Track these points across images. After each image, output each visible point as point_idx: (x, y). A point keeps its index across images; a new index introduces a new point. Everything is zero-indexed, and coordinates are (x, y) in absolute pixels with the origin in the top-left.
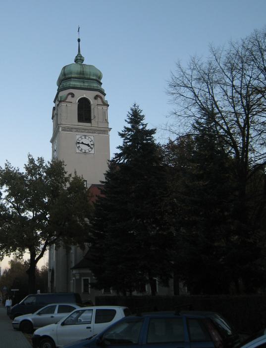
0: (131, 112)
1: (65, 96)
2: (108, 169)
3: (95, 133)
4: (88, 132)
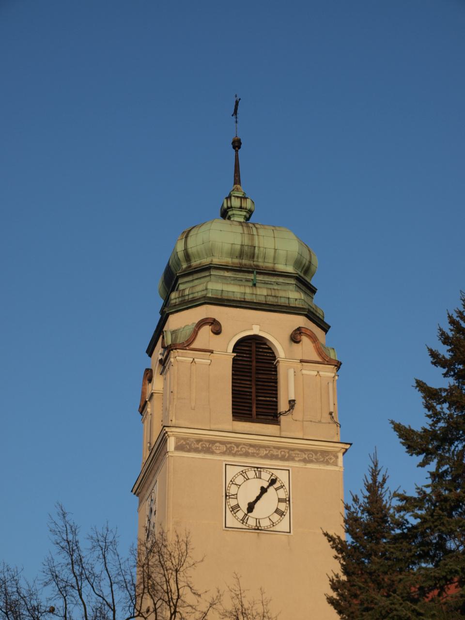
0: (430, 356)
1: (189, 332)
2: (336, 611)
3: (290, 459)
4: (266, 457)
